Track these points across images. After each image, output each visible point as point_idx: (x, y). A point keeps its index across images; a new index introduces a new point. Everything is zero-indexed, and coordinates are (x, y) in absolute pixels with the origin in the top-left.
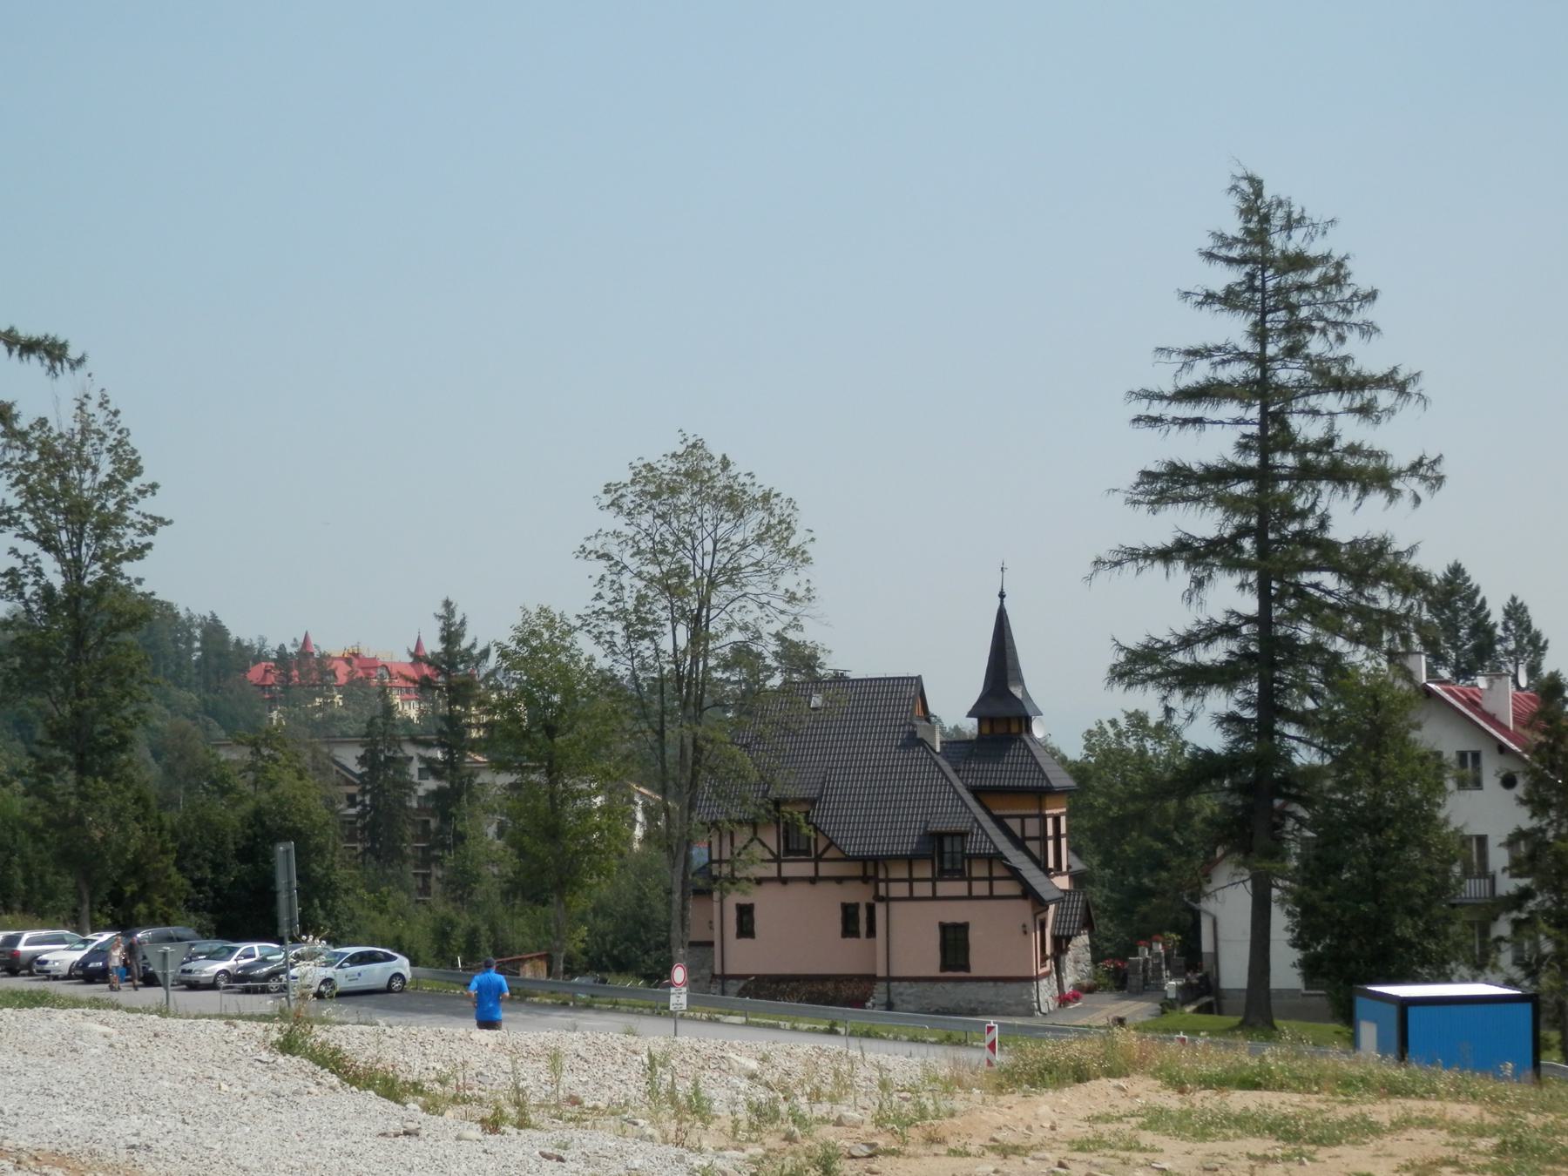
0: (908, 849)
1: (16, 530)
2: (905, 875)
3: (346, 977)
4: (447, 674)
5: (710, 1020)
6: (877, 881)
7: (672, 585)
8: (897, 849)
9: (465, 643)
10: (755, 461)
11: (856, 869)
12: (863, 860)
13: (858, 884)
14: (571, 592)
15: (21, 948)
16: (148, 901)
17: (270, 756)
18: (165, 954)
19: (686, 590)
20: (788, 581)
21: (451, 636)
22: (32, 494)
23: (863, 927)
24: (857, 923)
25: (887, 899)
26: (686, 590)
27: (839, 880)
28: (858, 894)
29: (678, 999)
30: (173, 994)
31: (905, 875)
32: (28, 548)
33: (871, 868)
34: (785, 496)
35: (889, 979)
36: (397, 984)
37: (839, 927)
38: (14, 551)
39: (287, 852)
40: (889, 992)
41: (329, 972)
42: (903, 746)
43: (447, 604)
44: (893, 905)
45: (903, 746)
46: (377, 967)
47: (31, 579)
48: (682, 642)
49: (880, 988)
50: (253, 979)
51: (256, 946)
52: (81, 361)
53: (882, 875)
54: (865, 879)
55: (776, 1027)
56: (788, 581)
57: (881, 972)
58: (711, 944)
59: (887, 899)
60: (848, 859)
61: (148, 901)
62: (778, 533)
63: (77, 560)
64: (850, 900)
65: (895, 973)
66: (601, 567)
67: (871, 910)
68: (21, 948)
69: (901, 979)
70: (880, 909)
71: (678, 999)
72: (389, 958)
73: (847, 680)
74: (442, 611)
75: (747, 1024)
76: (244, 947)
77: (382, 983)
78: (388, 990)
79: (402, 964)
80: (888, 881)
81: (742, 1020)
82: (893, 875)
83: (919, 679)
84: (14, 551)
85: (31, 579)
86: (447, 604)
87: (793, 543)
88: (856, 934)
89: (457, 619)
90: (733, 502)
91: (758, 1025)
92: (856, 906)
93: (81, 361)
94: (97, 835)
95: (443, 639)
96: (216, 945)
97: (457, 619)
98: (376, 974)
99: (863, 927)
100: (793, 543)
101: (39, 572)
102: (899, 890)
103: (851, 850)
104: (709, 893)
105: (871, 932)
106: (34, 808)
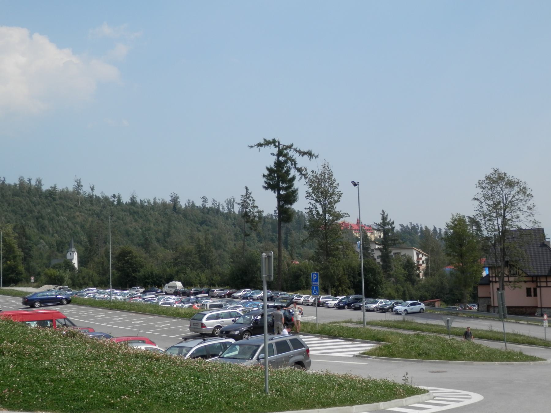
0: (546, 274)
1: (311, 198)
2: (545, 280)
3: (410, 309)
4: (383, 228)
5: (516, 322)
6: (537, 282)
7: (496, 206)
8: (542, 274)
9: (388, 220)
10: (512, 174)
11: (530, 279)
12: (532, 277)
13: (531, 283)
14: (469, 210)
15: (320, 300)
16: (342, 287)
17: (102, 220)
18: (448, 320)
19: (500, 208)
20: (530, 204)
21: (384, 218)
22: (314, 189)
23: (533, 294)
24: (531, 292)
25: (540, 287)
26: (500, 208)
27: (525, 282)
28: (532, 286)
29: (546, 324)
30: (507, 344)
31: (545, 280)
32: (313, 202)
33: (535, 279)
34: (523, 181)
35: (541, 308)
36: (422, 311)
37: (526, 294)
38: (310, 203)
39: (269, 257)
40: (542, 311)
41: (406, 308)
42: (541, 246)
43: (383, 211)
44: (542, 288)
45: (541, 246)
46: (417, 306)
47: (314, 209)
48: (500, 223)
49: (539, 311)
50: (385, 309)
51: (383, 300)
52: (318, 156)
53: (538, 280)
54: (533, 281)
55: (537, 325)
56: (530, 204)
57: (539, 306)
58: (490, 298)
59: (540, 287)
60: (528, 276)
61: (342, 287)
62: (523, 191)
63: (325, 204)
64: (528, 287)
65: (543, 306)
66: (477, 203)
67: (535, 290)
68: (320, 300)
69: (545, 308)
70: (538, 289)
71: (546, 324)
72: (420, 304)
73: (522, 229)
74: (382, 213)
75: (528, 324)
76: (380, 300)
77: (418, 310)
78: (420, 312)
79: (423, 306)
80: (540, 282)
81: (526, 322)
82: (542, 280)
83: (543, 229)
84: (310, 203)
85: (314, 209)
86: (383, 211)
87: (528, 193)
88: (530, 296)
89: (386, 215)
90: (511, 184)
91: (532, 324)
92: (530, 289)
93: (318, 156)
94: (332, 271)
95: (382, 219)
96: (372, 300)
97: (386, 215)
98: (417, 308)
99: (533, 294)
100: (528, 193)
101: (316, 208)
102: (544, 284)
103: (530, 274)
104: (489, 284)
105: (535, 295)
106: (317, 265)
